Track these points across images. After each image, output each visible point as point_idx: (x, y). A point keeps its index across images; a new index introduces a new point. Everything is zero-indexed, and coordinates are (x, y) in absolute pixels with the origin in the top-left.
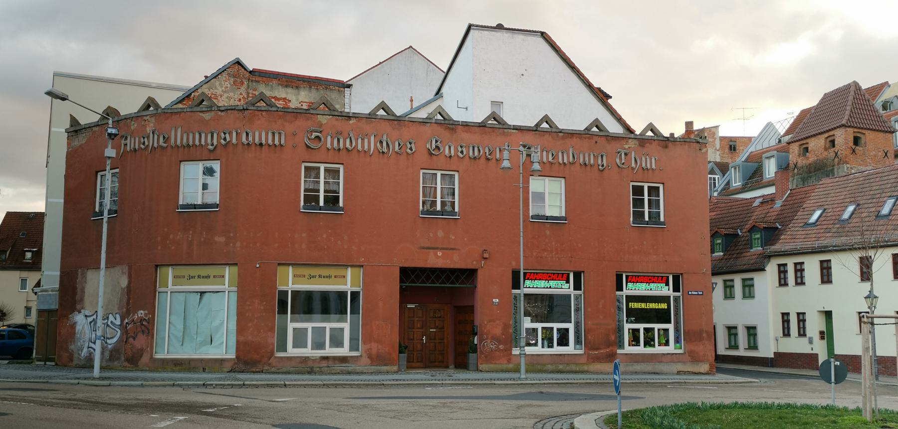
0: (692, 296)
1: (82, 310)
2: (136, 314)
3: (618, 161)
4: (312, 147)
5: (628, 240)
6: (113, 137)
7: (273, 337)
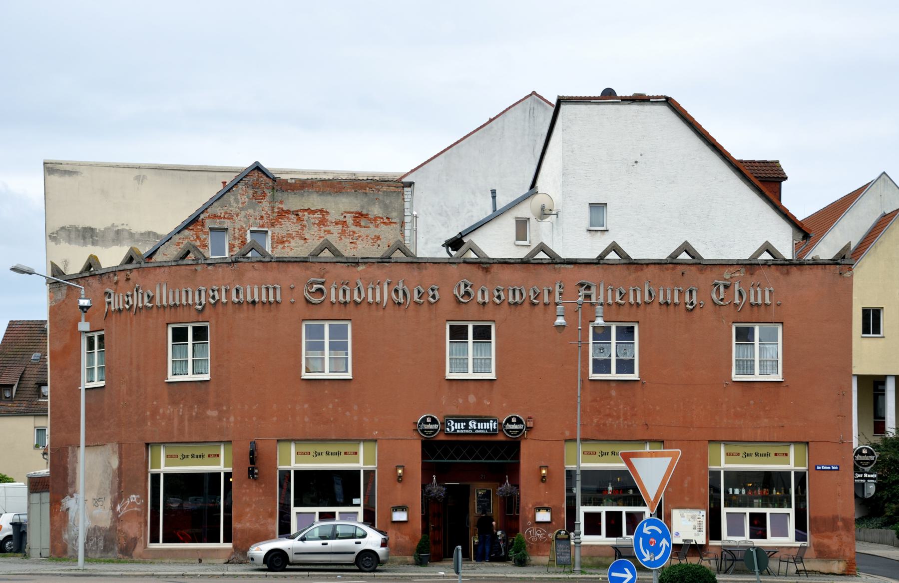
0: (833, 471)
1: (74, 494)
2: (128, 499)
3: (714, 296)
4: (313, 302)
5: (727, 400)
6: (85, 310)
7: (274, 524)
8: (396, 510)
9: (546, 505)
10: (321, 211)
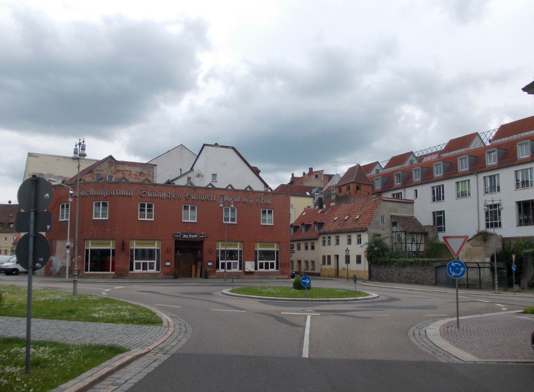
8: (167, 262)
9: (211, 260)
10: (130, 171)
